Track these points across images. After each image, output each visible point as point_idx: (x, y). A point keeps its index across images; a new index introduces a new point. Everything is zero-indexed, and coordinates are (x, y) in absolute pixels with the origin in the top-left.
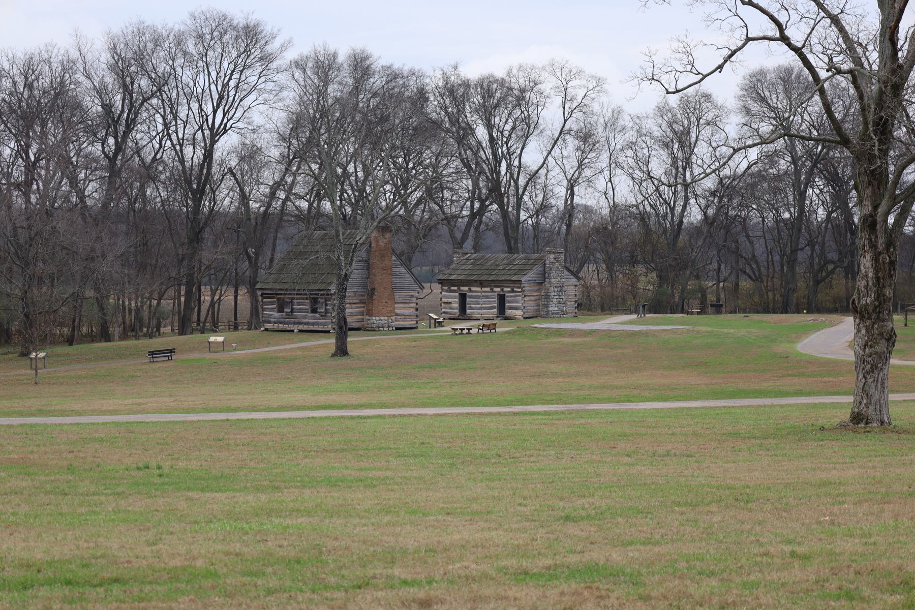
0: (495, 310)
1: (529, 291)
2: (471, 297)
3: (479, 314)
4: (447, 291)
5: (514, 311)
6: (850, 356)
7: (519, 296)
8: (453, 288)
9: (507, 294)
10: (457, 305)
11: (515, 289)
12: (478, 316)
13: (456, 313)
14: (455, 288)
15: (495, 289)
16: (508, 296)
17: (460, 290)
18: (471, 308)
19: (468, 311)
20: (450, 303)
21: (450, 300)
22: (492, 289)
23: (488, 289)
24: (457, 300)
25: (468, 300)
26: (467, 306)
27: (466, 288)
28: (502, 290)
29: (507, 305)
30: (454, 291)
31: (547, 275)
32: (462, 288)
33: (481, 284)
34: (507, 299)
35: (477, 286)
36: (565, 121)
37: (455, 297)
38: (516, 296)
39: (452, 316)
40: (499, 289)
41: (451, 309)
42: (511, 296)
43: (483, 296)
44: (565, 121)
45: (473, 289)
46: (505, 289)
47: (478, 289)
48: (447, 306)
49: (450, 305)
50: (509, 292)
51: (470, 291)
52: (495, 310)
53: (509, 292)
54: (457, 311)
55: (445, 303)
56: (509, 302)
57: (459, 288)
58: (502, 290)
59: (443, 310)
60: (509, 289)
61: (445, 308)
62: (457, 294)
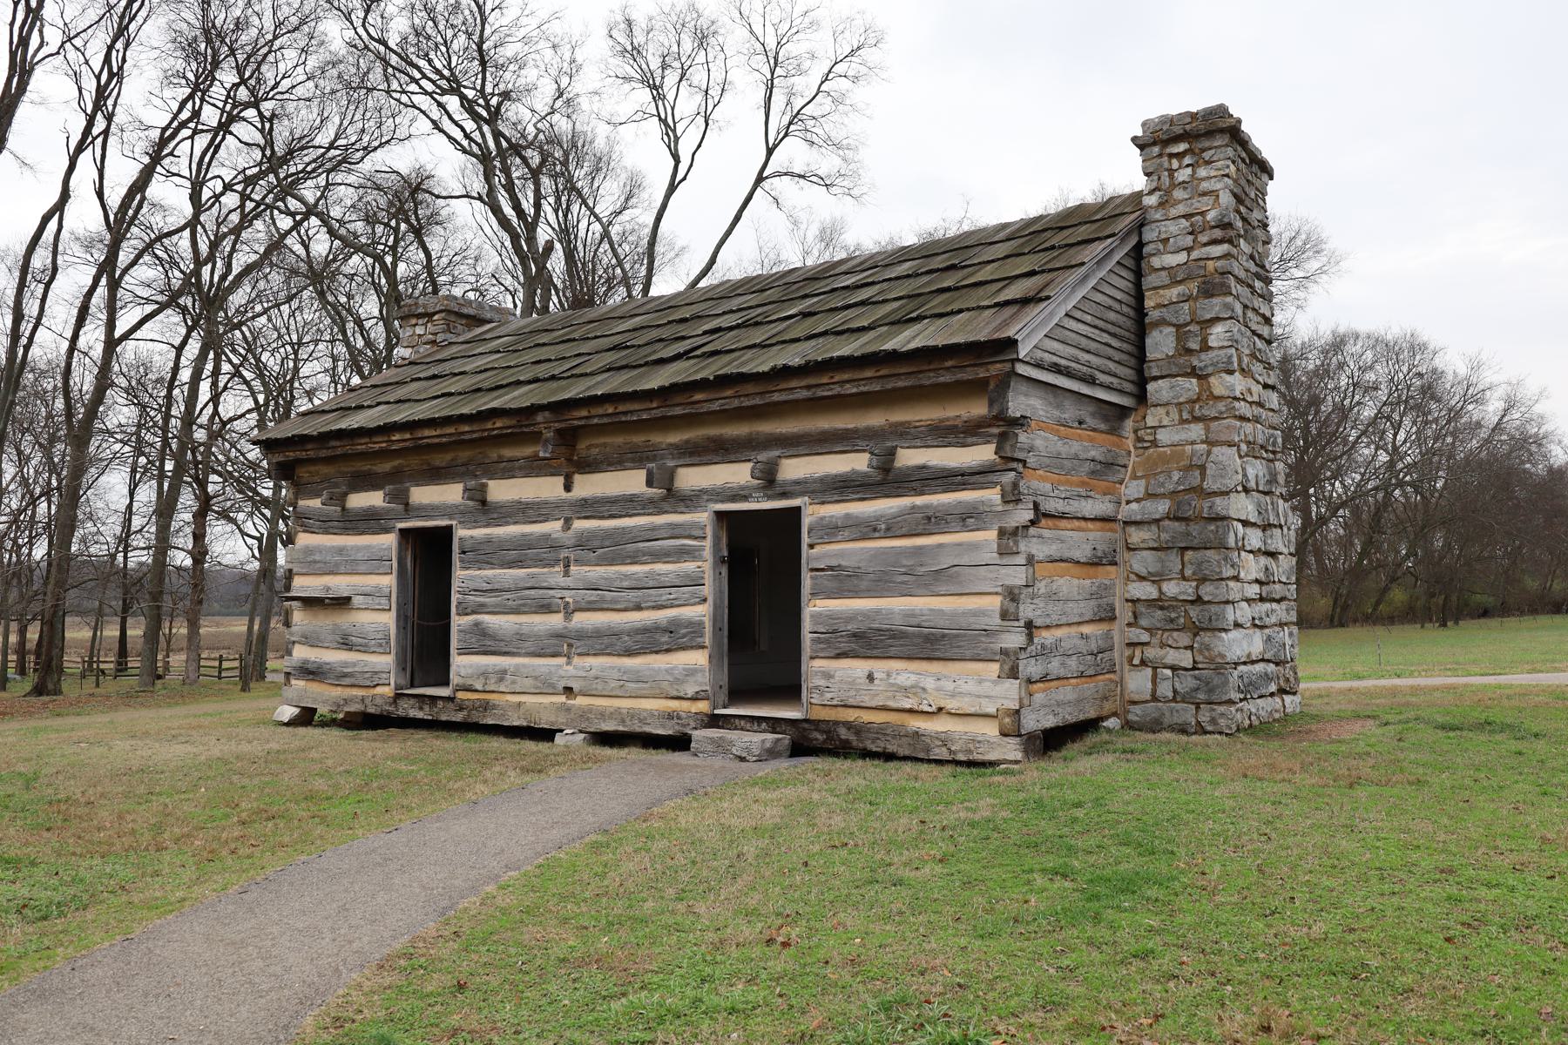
0: (699, 658)
1: (1056, 464)
2: (483, 555)
3: (545, 686)
4: (326, 525)
5: (903, 673)
6: (68, 619)
7: (968, 517)
8: (360, 500)
9: (813, 513)
10: (387, 620)
11: (910, 457)
12: (540, 708)
13: (373, 679)
14: (372, 499)
15: (692, 478)
16: (831, 531)
17: (408, 509)
18: (486, 643)
19: (462, 665)
20: (342, 603)
21: (340, 584)
22: (663, 480)
23: (632, 482)
24: (388, 582)
25: (461, 576)
26: (458, 622)
27: (451, 493)
28: (768, 479)
29: (816, 608)
30: (369, 522)
31: (1161, 344)
32: (422, 495)
33: (568, 437)
34: (814, 554)
35: (535, 468)
36: (770, 152)
37: (375, 563)
38: (932, 522)
39: (356, 698)
40: (738, 474)
41: (346, 644)
42: (868, 529)
43: (585, 544)
44: (770, 152)
45: (502, 491)
46: (795, 469)
47: (548, 488)
48: (324, 622)
49: (346, 620)
50: (843, 487)
51: (483, 508)
52: (699, 658)
53: (843, 487)
54: (385, 662)
55: (310, 603)
56: (843, 581)
57: (400, 497)
58: (768, 479)
59: (301, 653)
60: (857, 462)
61: (310, 641)
62: (389, 541)
